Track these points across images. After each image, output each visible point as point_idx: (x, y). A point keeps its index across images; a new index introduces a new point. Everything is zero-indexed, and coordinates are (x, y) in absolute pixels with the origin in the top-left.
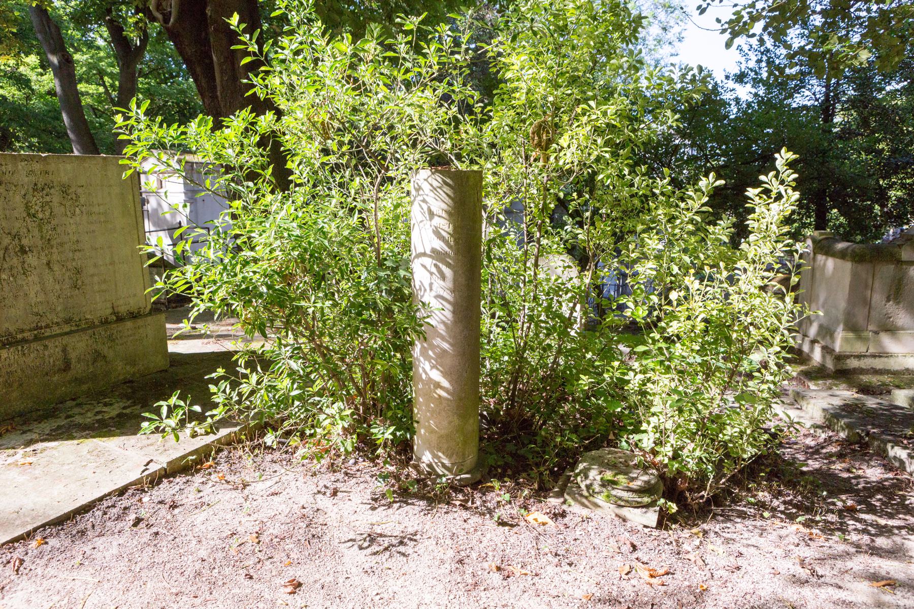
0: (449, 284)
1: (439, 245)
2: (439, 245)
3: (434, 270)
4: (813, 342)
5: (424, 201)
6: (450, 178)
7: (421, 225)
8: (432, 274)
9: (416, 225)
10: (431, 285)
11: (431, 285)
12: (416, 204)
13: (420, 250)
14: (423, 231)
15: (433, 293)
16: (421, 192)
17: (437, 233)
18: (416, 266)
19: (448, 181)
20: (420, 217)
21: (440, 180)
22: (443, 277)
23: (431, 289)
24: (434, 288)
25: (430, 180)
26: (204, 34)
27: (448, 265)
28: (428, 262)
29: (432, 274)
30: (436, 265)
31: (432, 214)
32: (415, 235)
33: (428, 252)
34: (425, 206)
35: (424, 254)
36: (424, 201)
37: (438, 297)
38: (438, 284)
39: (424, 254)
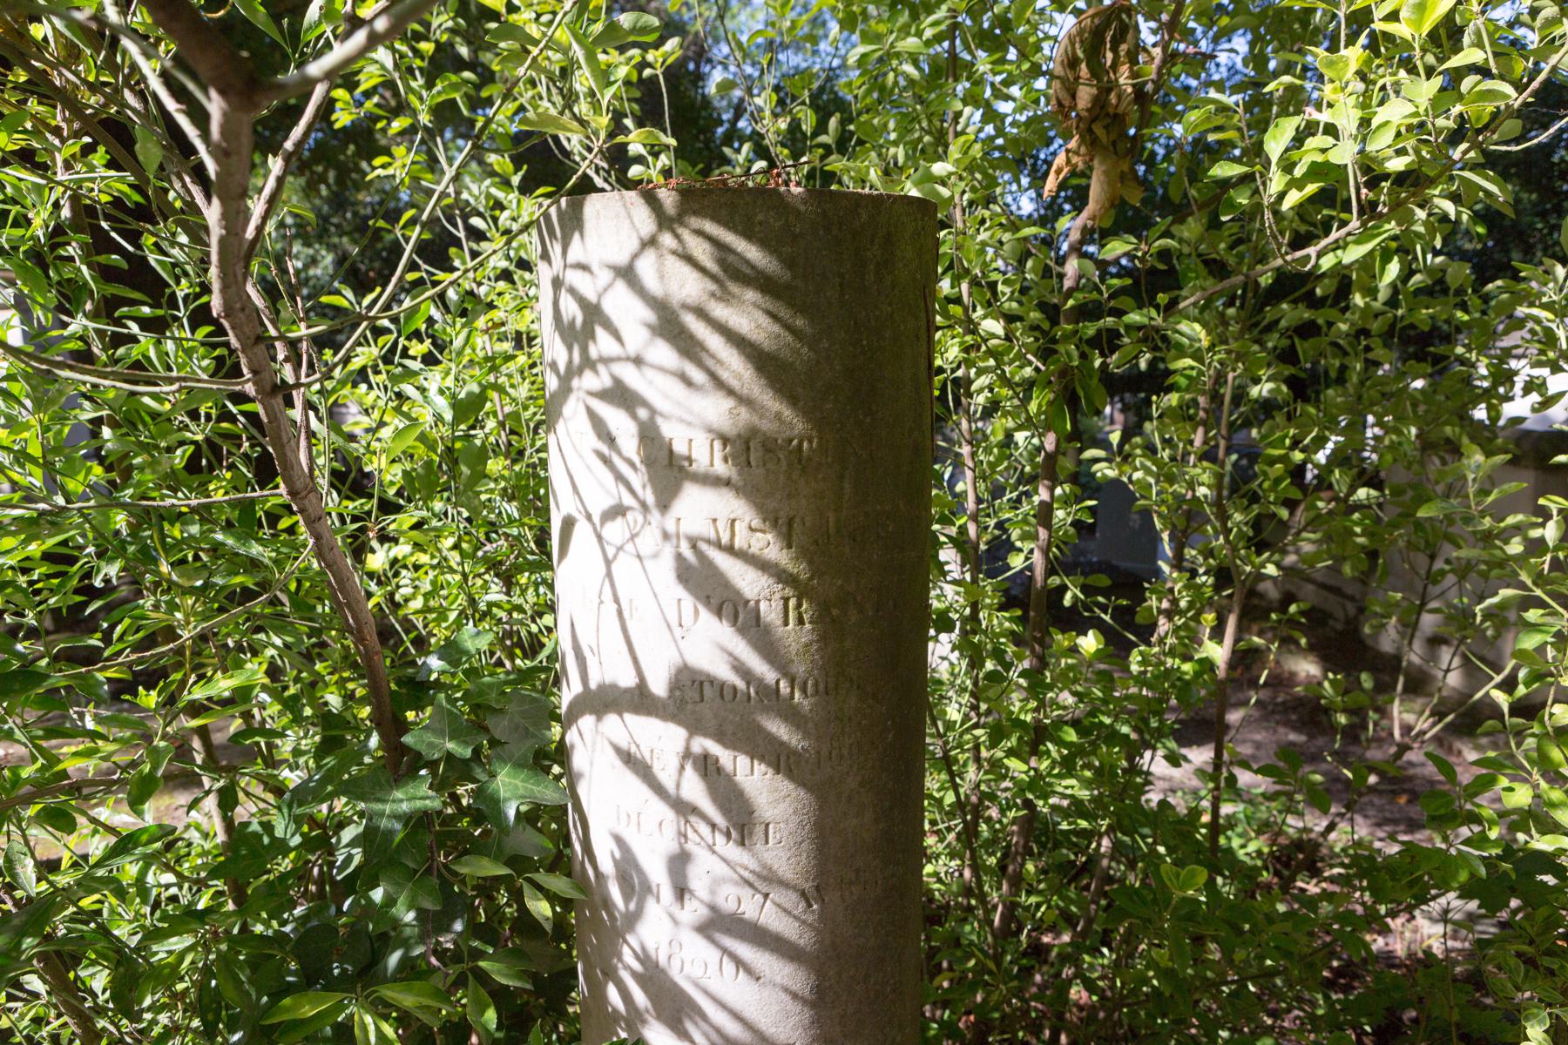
0: (783, 849)
1: (713, 647)
2: (713, 647)
3: (694, 789)
4: (1435, 641)
5: (621, 396)
6: (763, 243)
7: (615, 531)
8: (684, 809)
9: (582, 531)
10: (679, 863)
11: (679, 863)
12: (573, 410)
13: (613, 670)
14: (625, 568)
15: (693, 911)
16: (603, 344)
17: (701, 580)
18: (592, 745)
19: (752, 252)
20: (600, 491)
21: (701, 251)
22: (741, 821)
23: (681, 892)
24: (698, 881)
25: (646, 268)
26: (1094, 845)
27: (779, 759)
28: (663, 741)
29: (684, 809)
30: (707, 767)
31: (668, 471)
32: (575, 576)
33: (659, 686)
34: (620, 423)
35: (639, 700)
36: (621, 396)
37: (718, 925)
38: (718, 869)
39: (639, 700)
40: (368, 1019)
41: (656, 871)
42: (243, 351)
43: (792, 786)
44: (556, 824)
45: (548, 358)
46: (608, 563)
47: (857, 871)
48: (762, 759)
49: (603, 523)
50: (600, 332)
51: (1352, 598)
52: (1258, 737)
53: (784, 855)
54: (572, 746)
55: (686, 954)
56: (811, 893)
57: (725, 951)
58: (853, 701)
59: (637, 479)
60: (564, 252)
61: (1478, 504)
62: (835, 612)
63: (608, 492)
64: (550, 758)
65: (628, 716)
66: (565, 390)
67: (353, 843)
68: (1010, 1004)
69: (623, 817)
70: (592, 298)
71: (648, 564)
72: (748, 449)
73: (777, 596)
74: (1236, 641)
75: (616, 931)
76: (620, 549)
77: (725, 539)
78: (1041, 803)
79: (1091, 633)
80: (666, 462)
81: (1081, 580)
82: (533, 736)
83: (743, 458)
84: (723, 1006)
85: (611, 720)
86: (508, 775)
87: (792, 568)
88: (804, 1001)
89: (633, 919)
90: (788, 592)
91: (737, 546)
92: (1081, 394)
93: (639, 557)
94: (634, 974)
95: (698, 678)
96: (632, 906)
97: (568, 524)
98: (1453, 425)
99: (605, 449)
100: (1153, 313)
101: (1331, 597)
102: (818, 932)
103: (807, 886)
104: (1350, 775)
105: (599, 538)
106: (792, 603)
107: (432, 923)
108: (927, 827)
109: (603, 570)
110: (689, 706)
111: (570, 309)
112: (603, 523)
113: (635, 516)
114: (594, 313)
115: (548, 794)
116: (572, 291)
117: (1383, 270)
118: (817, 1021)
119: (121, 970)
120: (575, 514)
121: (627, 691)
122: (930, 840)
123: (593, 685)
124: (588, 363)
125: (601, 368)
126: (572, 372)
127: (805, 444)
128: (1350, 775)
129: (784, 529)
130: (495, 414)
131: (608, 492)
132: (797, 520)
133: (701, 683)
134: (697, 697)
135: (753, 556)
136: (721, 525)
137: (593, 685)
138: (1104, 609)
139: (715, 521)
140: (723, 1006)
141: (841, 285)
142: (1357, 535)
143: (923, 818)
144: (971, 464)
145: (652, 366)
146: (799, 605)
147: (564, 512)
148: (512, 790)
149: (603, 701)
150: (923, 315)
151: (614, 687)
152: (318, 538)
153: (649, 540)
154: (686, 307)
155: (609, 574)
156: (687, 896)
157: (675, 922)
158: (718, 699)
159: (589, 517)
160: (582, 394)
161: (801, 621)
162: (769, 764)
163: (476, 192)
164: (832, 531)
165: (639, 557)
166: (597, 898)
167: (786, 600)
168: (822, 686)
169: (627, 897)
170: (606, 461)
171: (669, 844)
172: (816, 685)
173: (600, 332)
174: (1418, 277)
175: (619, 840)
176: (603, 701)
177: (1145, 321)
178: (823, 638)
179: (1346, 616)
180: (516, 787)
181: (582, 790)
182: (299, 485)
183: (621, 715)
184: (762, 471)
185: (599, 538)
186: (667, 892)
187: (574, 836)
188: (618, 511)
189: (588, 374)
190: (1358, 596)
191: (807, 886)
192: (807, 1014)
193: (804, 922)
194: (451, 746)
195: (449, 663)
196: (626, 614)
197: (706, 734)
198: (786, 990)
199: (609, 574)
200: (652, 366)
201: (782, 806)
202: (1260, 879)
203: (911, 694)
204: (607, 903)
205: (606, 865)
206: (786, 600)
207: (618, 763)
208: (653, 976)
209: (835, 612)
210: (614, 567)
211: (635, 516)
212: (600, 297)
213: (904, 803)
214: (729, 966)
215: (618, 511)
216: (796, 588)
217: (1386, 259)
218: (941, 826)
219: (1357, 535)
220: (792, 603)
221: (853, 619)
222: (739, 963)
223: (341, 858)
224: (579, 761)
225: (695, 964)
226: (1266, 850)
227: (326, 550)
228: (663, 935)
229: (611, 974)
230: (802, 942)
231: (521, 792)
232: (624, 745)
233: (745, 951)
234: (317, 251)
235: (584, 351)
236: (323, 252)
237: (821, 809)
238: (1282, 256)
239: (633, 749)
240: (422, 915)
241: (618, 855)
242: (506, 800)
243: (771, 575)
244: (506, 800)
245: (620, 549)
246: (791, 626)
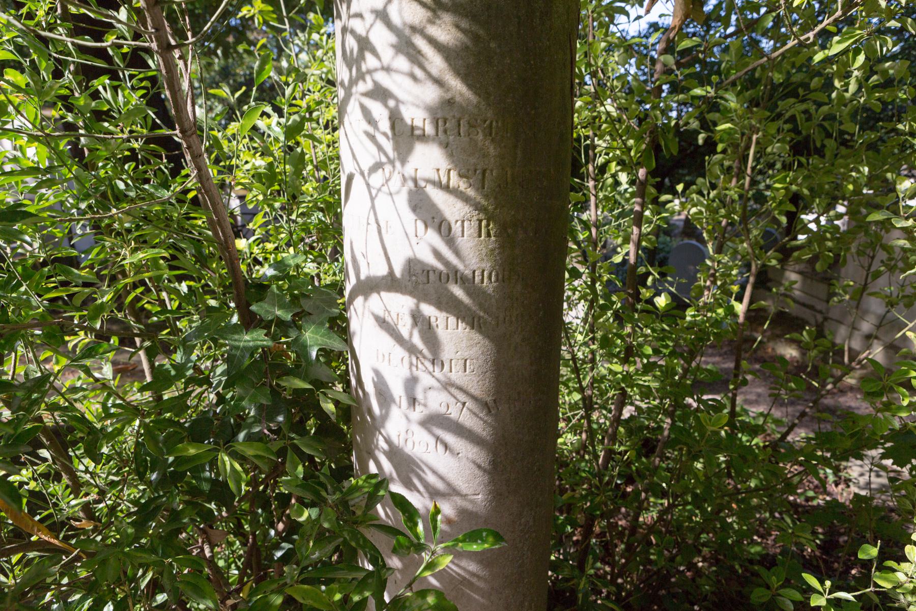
5: (380, 93)
7: (377, 179)
9: (358, 182)
10: (411, 383)
12: (353, 109)
14: (382, 201)
15: (418, 413)
16: (370, 61)
18: (362, 317)
34: (379, 111)
35: (390, 283)
37: (433, 422)
40: (226, 458)
41: (397, 390)
42: (148, 11)
43: (481, 338)
44: (340, 359)
45: (339, 80)
46: (372, 199)
47: (519, 393)
48: (463, 320)
49: (369, 174)
50: (368, 56)
51: (820, 312)
52: (759, 390)
53: (476, 379)
54: (354, 333)
55: (416, 438)
56: (491, 404)
57: (438, 438)
58: (519, 287)
59: (388, 146)
60: (348, 7)
61: (905, 213)
62: (510, 231)
63: (374, 157)
64: (340, 326)
65: (383, 294)
66: (348, 96)
67: (222, 374)
68: (606, 506)
69: (381, 357)
70: (364, 34)
71: (395, 197)
72: (459, 125)
73: (475, 218)
74: (751, 302)
75: (376, 425)
76: (379, 190)
77: (444, 181)
78: (629, 390)
79: (663, 295)
80: (409, 134)
81: (659, 269)
82: (328, 312)
83: (456, 131)
84: (434, 472)
85: (374, 297)
86: (312, 332)
87: (484, 202)
88: (485, 471)
89: (385, 417)
90: (482, 216)
91: (451, 186)
92: (663, 143)
93: (391, 194)
94: (385, 453)
95: (426, 268)
96: (384, 411)
97: (350, 178)
98: (892, 173)
99: (370, 130)
100: (709, 89)
101: (808, 310)
102: (494, 428)
103: (489, 399)
104: (817, 385)
105: (368, 185)
106: (484, 223)
107: (267, 414)
108: (561, 415)
109: (370, 204)
110: (421, 286)
111: (351, 43)
112: (369, 174)
113: (388, 168)
114: (365, 44)
115: (336, 344)
116: (353, 32)
117: (854, 59)
118: (492, 482)
119: (90, 437)
120: (354, 172)
121: (384, 278)
122: (562, 425)
123: (363, 277)
124: (361, 76)
125: (368, 78)
126: (353, 82)
127: (494, 123)
128: (817, 385)
129: (480, 177)
130: (312, 161)
131: (374, 157)
132: (488, 171)
133: (428, 272)
134: (425, 280)
135: (461, 192)
136: (442, 173)
137: (363, 277)
138: (671, 284)
139: (438, 170)
140: (434, 472)
141: (519, 23)
142: (828, 240)
143: (558, 412)
144: (594, 192)
145: (402, 73)
146: (488, 225)
147: (347, 172)
148: (314, 339)
149: (368, 287)
150: (568, 52)
151: (375, 278)
152: (199, 169)
153: (395, 183)
154: (428, 181)
155: (373, 207)
156: (417, 404)
157: (407, 418)
158: (438, 282)
159: (362, 173)
160: (358, 96)
161: (489, 235)
162: (467, 324)
163: (303, 39)
164: (509, 180)
165: (391, 194)
166: (364, 408)
167: (480, 221)
168: (500, 276)
169: (381, 405)
170: (372, 138)
171: (405, 372)
172: (497, 275)
173: (368, 56)
174: (875, 77)
175: (377, 372)
176: (368, 287)
177: (704, 93)
178: (502, 247)
179: (816, 321)
180: (317, 339)
181: (356, 344)
182: (186, 126)
183: (379, 293)
184: (467, 139)
185: (368, 185)
186: (404, 403)
187: (351, 374)
188: (377, 166)
189: (361, 83)
190: (824, 311)
191: (489, 399)
192: (486, 478)
193: (485, 422)
194: (279, 313)
195: (280, 272)
196: (383, 231)
197: (430, 302)
198: (474, 462)
199: (373, 207)
200: (402, 73)
201: (475, 349)
202: (753, 504)
203: (552, 328)
204: (370, 411)
205: (369, 388)
206: (480, 221)
207: (378, 328)
208: (394, 453)
209: (510, 231)
210: (376, 202)
211: (388, 168)
212: (368, 32)
213: (544, 383)
214: (441, 448)
215: (377, 166)
216: (486, 214)
217: (857, 52)
218: (569, 414)
219: (828, 240)
220: (484, 223)
221: (521, 236)
222: (446, 446)
223: (215, 383)
224: (354, 325)
225: (421, 445)
226: (761, 445)
227: (204, 179)
228: (400, 428)
229: (371, 455)
230: (485, 433)
231: (320, 342)
232: (381, 313)
233: (450, 438)
234: (213, 103)
235: (359, 69)
236: (216, 104)
237: (498, 352)
238: (796, 37)
239: (388, 319)
240: (260, 408)
241: (376, 379)
242: (311, 346)
243: (471, 205)
244: (311, 346)
245: (379, 190)
246: (483, 237)
